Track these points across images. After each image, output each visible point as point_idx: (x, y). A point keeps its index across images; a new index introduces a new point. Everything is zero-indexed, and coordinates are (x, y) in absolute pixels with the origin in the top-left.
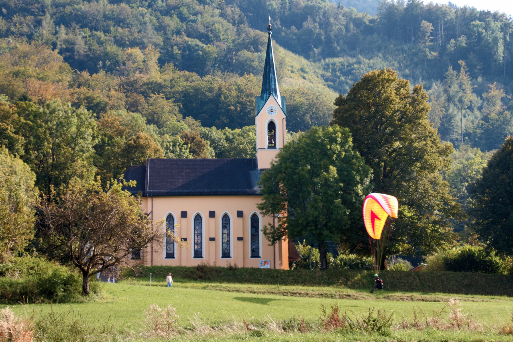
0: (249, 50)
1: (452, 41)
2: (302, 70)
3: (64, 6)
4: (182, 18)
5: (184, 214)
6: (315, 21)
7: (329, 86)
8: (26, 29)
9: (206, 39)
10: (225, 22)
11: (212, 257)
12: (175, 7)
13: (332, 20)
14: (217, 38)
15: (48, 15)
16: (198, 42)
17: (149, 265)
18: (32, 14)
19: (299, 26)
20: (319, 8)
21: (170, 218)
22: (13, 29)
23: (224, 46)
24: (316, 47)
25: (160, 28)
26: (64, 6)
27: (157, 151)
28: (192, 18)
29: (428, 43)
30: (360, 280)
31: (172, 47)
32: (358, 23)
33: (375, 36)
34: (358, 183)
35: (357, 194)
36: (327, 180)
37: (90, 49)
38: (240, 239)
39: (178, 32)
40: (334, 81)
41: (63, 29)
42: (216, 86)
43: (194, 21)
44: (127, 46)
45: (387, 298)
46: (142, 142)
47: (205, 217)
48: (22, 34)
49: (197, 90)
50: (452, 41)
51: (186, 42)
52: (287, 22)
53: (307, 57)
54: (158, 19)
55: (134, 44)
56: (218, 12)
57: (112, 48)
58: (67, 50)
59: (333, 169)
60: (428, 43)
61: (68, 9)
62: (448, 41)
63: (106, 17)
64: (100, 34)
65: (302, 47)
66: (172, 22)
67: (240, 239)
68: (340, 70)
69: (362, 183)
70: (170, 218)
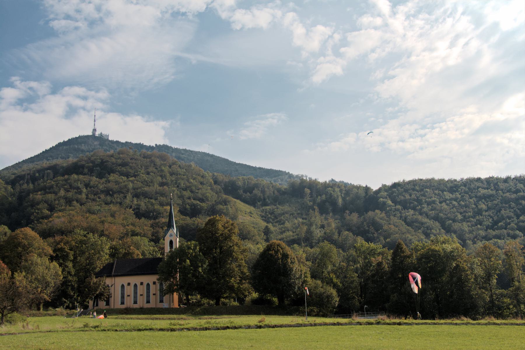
0: (221, 204)
1: (319, 197)
2: (250, 213)
3: (137, 189)
4: (192, 192)
5: (142, 284)
6: (258, 190)
7: (263, 220)
8: (119, 200)
9: (202, 200)
10: (212, 193)
11: (129, 303)
12: (189, 187)
13: (266, 189)
14: (208, 200)
15: (130, 194)
16: (198, 202)
17: (112, 307)
18: (123, 193)
19: (251, 192)
20: (261, 184)
21: (123, 286)
22: (113, 200)
23: (210, 203)
24: (259, 202)
25: (181, 197)
26: (137, 189)
27: (138, 255)
28: (197, 191)
29: (308, 198)
30: (199, 311)
31: (186, 205)
32: (279, 190)
33: (286, 195)
34: (200, 267)
35: (199, 272)
36: (184, 266)
37: (147, 208)
38: (154, 294)
39: (189, 198)
40: (265, 217)
41: (135, 199)
42: (196, 222)
43: (197, 193)
44: (165, 205)
45: (200, 319)
46: (131, 251)
47: (138, 285)
48: (117, 203)
49: (187, 225)
50: (319, 197)
51: (192, 202)
52: (245, 191)
53: (255, 207)
54: (180, 192)
55: (167, 204)
56: (209, 188)
57: (157, 207)
58: (137, 209)
59: (188, 261)
60: (308, 198)
61: (139, 190)
62: (317, 197)
63: (157, 193)
64: (153, 201)
65: (252, 202)
66: (187, 194)
67: (141, 295)
68: (269, 212)
69: (202, 266)
70: (123, 286)
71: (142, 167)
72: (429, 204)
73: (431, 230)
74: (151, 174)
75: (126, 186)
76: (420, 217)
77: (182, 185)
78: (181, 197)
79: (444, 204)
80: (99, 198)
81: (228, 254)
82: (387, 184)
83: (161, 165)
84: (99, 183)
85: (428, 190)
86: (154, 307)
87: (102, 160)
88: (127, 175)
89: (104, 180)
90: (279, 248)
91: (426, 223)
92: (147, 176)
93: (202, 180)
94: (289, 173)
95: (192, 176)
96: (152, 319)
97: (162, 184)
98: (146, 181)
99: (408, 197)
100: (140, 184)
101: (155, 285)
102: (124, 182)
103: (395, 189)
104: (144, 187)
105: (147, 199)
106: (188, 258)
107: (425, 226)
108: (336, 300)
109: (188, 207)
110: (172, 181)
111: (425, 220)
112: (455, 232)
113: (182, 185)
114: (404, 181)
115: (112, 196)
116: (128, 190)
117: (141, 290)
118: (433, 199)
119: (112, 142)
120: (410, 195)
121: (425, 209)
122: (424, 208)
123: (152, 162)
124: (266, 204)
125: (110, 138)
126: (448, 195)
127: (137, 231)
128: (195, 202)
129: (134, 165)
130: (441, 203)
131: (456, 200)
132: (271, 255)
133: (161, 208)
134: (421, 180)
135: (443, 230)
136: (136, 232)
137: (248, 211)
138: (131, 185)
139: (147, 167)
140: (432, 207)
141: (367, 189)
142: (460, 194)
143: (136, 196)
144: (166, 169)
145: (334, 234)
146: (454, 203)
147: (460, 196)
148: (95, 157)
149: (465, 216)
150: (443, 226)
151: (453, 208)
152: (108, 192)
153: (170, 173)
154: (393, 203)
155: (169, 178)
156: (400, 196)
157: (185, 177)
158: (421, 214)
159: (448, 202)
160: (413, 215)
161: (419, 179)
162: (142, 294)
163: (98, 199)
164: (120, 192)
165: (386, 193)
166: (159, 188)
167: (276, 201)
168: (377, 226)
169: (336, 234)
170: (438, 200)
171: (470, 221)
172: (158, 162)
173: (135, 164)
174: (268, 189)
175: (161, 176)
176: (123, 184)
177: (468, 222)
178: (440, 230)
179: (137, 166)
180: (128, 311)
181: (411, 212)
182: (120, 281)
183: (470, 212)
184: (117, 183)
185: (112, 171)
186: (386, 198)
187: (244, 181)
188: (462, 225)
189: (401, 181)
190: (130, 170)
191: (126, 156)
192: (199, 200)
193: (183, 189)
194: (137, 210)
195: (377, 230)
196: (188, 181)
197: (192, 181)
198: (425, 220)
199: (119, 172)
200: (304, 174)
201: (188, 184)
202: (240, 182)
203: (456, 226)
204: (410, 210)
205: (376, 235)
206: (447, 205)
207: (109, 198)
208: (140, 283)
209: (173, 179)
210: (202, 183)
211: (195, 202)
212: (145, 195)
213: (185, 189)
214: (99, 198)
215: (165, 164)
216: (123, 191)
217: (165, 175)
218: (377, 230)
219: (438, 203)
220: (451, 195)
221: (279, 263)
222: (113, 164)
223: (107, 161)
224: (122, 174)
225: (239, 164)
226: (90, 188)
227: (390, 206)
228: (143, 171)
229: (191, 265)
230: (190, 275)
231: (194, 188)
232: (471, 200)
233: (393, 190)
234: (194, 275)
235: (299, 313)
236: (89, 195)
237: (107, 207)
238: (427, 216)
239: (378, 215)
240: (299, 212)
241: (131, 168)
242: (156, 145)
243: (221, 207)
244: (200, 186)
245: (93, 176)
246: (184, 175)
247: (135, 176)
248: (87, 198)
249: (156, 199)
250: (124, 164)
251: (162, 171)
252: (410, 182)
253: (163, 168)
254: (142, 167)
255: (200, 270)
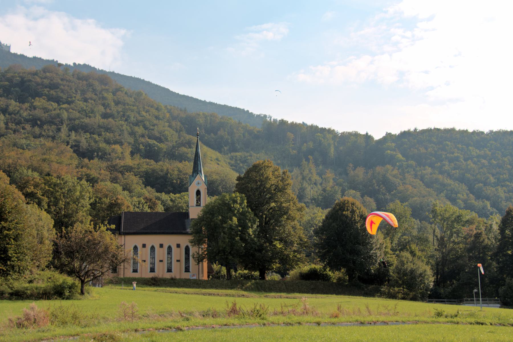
0: (185, 147)
2: (217, 159)
3: (75, 120)
4: (145, 128)
5: (144, 246)
6: (225, 131)
7: (233, 169)
8: (51, 133)
12: (142, 121)
13: (235, 130)
14: (167, 139)
15: (65, 125)
16: (155, 142)
17: (122, 277)
18: (56, 124)
21: (136, 248)
22: (43, 133)
23: (171, 145)
25: (132, 134)
26: (75, 120)
27: (128, 207)
28: (152, 127)
29: (292, 145)
30: (250, 286)
31: (139, 145)
35: (249, 234)
36: (231, 225)
37: (89, 145)
38: (178, 261)
39: (143, 136)
40: (236, 166)
41: (73, 133)
46: (119, 201)
48: (49, 136)
49: (154, 170)
50: (305, 144)
51: (148, 142)
53: (220, 152)
54: (131, 128)
56: (167, 124)
57: (103, 145)
58: (75, 146)
60: (292, 145)
61: (77, 122)
63: (100, 126)
64: (96, 136)
65: (217, 146)
66: (139, 130)
67: (178, 261)
68: (240, 160)
70: (136, 248)
71: (76, 91)
72: (451, 161)
73: (456, 194)
74: (90, 101)
75: (58, 115)
76: (440, 177)
77: (132, 118)
78: (132, 134)
79: (469, 162)
80: (24, 128)
81: (282, 212)
82: (393, 133)
83: (102, 90)
84: (21, 109)
85: (449, 143)
86: (197, 278)
87: (22, 78)
88: (58, 100)
89: (27, 105)
90: (355, 209)
91: (450, 185)
92: (85, 103)
93: (156, 113)
94: (248, 111)
95: (144, 108)
96: (204, 294)
97: (105, 116)
98: (85, 111)
99: (423, 150)
100: (78, 115)
102: (55, 110)
103: (406, 140)
104: (83, 118)
105: (88, 134)
107: (449, 188)
108: (430, 280)
109: (141, 147)
110: (118, 112)
111: (448, 181)
112: (488, 199)
113: (132, 118)
114: (416, 129)
115: (41, 127)
116: (62, 120)
118: (456, 155)
119: (15, 55)
120: (426, 149)
121: (446, 168)
122: (444, 165)
123: (90, 85)
124: (235, 150)
125: (12, 51)
126: (475, 152)
127: (93, 176)
128: (151, 142)
129: (66, 88)
130: (466, 160)
131: (485, 157)
132: (347, 217)
134: (438, 130)
135: (471, 195)
136: (91, 177)
137: (214, 157)
138: (65, 115)
139: (83, 92)
140: (455, 164)
141: (368, 137)
142: (490, 151)
143: (73, 128)
144: (109, 96)
145: (336, 192)
146: (483, 161)
147: (490, 153)
148: (12, 74)
149: (498, 179)
150: (471, 190)
151: (482, 168)
152: (34, 122)
153: (114, 101)
154: (403, 157)
155: (114, 109)
156: (412, 149)
157: (135, 108)
158: (441, 173)
159: (475, 159)
160: (431, 174)
161: (435, 129)
162: (179, 259)
163: (22, 130)
164: (51, 122)
165: (394, 145)
166: (102, 120)
168: (390, 187)
169: (339, 193)
170: (462, 156)
171: (507, 186)
172: (98, 87)
173: (68, 86)
175: (103, 105)
176: (53, 112)
177: (502, 186)
178: (467, 195)
179: (71, 89)
181: (429, 170)
183: (505, 174)
184: (46, 110)
185: (37, 94)
186: (395, 150)
187: (206, 118)
188: (497, 190)
189: (412, 129)
190: (61, 95)
191: (55, 75)
193: (133, 124)
194: (76, 148)
195: (389, 191)
196: (139, 114)
197: (144, 113)
198: (448, 181)
199: (46, 95)
200: (267, 114)
201: (140, 118)
202: (201, 120)
203: (489, 191)
204: (427, 167)
205: (388, 197)
206: (474, 163)
207: (37, 130)
208: (141, 245)
209: (120, 110)
210: (157, 118)
211: (151, 142)
212: (85, 128)
213: (137, 124)
214: (24, 128)
215: (107, 90)
216: (55, 121)
217: (108, 104)
218: (389, 191)
219: (462, 160)
220: (478, 151)
221: (357, 228)
222: (38, 84)
223: (30, 81)
224: (50, 99)
225: (184, 96)
226: (10, 114)
227: (400, 161)
228: (78, 96)
230: (238, 238)
231: (147, 123)
232: (506, 159)
233: (404, 140)
235: (381, 293)
236: (9, 124)
237: (37, 141)
238: (450, 176)
239: (391, 172)
240: (279, 161)
241: (62, 91)
242: (74, 64)
244: (155, 122)
245: (11, 99)
246: (133, 106)
247: (69, 103)
248: (7, 128)
250: (54, 86)
251: (104, 98)
252: (423, 132)
253: (106, 95)
254: (76, 91)
255: (250, 231)
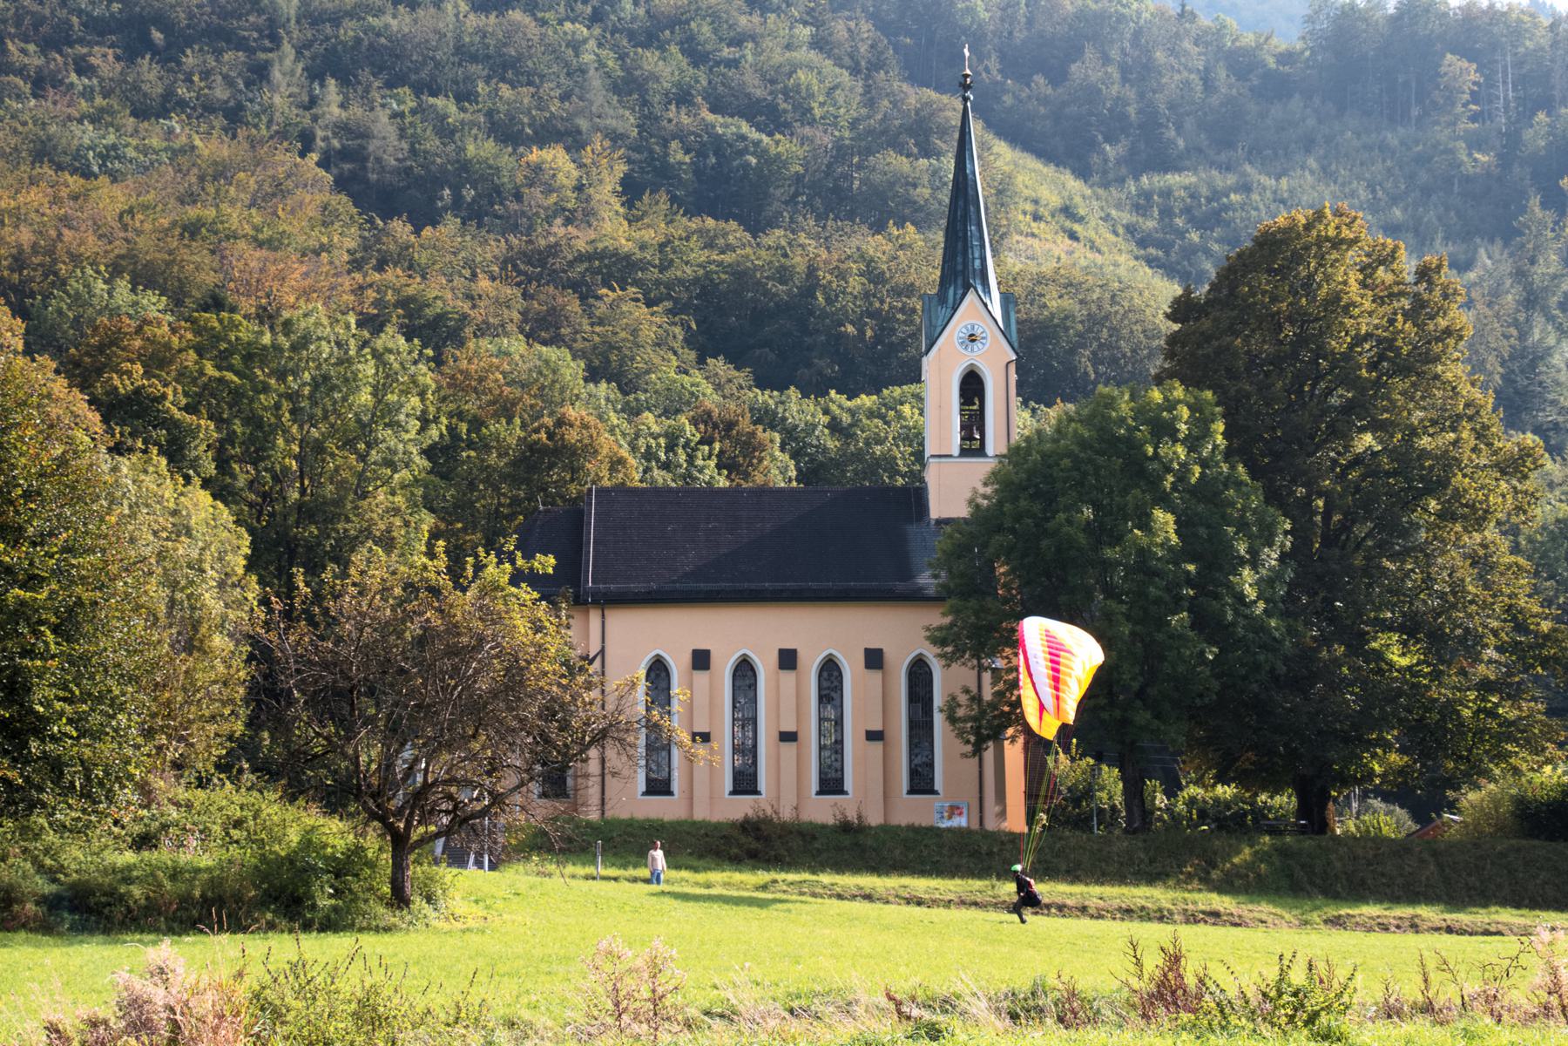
0: (901, 150)
2: (1067, 211)
3: (336, 21)
4: (696, 56)
5: (701, 660)
6: (1106, 60)
7: (1151, 262)
8: (221, 93)
9: (769, 117)
11: (787, 790)
15: (288, 49)
17: (594, 816)
18: (241, 44)
21: (658, 671)
22: (181, 91)
25: (629, 86)
27: (617, 463)
28: (727, 52)
30: (1249, 866)
31: (665, 143)
33: (1296, 103)
35: (1240, 597)
36: (1144, 553)
37: (413, 151)
38: (873, 736)
39: (683, 98)
40: (1166, 246)
42: (799, 262)
43: (734, 63)
44: (528, 142)
45: (1336, 922)
46: (572, 436)
48: (209, 108)
49: (740, 274)
51: (708, 128)
52: (1018, 64)
53: (1083, 173)
54: (622, 57)
55: (546, 135)
56: (805, 32)
57: (480, 148)
59: (1164, 520)
61: (349, 30)
66: (665, 67)
68: (1187, 210)
69: (1255, 564)
70: (658, 671)
78: (629, 86)
80: (83, 68)
81: (1414, 481)
101: (875, 677)
105: (404, 91)
106: (1164, 501)
115: (168, 57)
117: (785, 701)
133: (506, 160)
137: (1052, 199)
143: (330, 64)
167: (1225, 136)
174: (1172, 52)
180: (760, 845)
182: (668, 632)
192: (750, 119)
207: (149, 74)
213: (650, 38)
214: (83, 68)
229: (1188, 550)
234: (1205, 623)
243: (898, 163)
249: (464, 97)
